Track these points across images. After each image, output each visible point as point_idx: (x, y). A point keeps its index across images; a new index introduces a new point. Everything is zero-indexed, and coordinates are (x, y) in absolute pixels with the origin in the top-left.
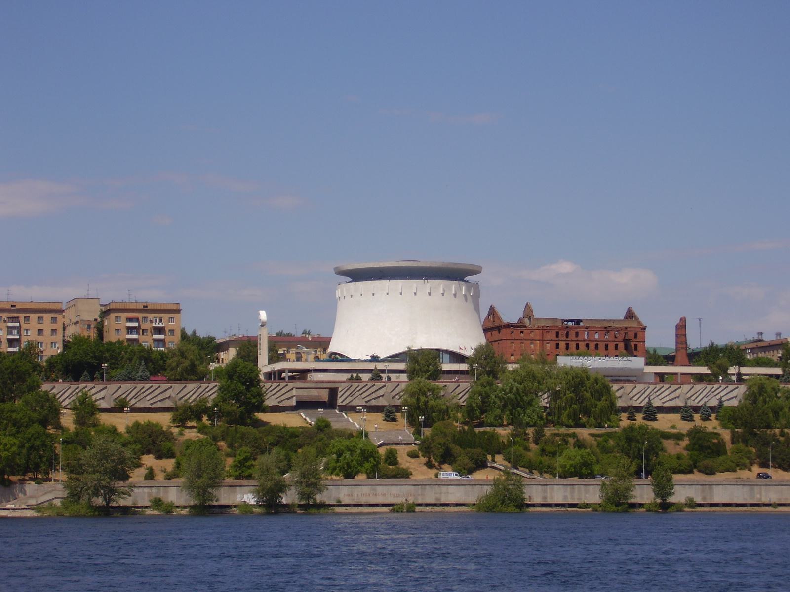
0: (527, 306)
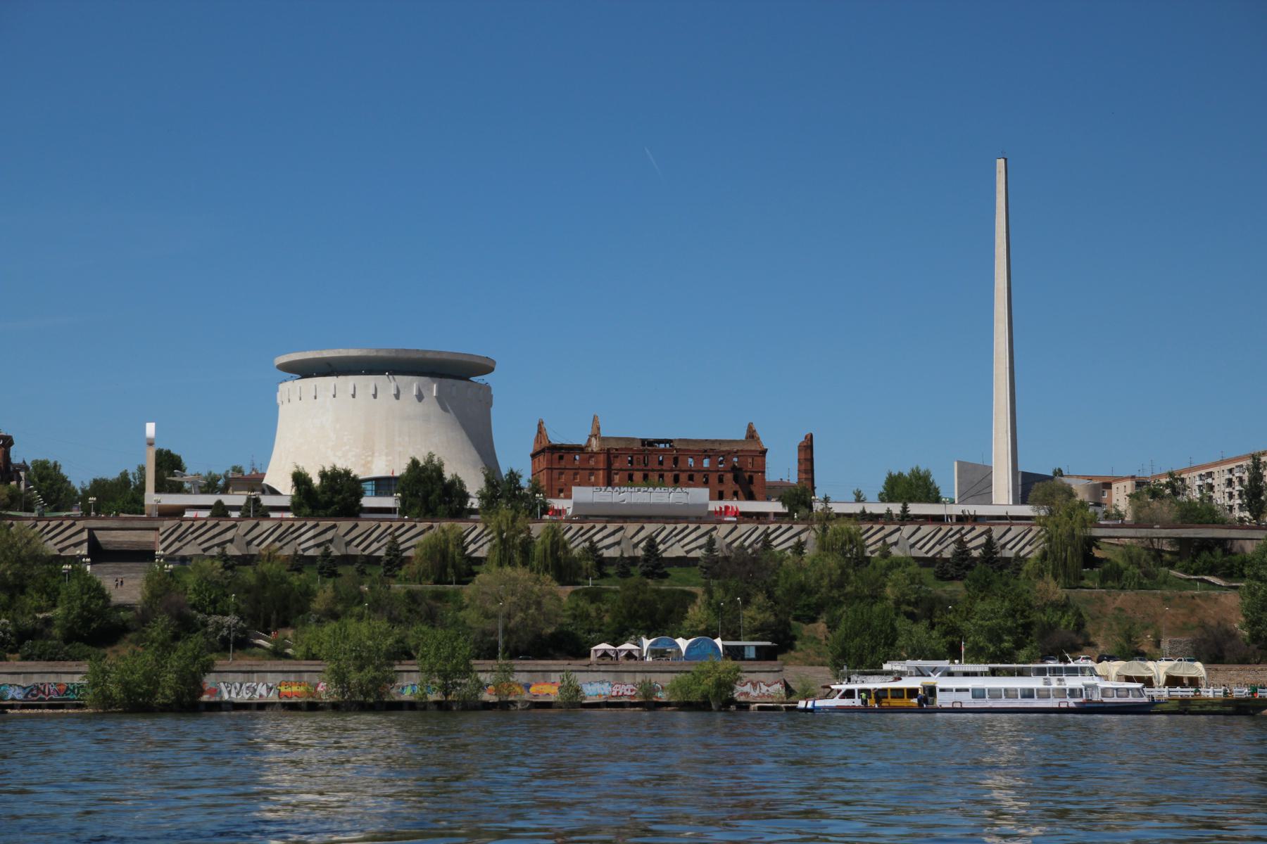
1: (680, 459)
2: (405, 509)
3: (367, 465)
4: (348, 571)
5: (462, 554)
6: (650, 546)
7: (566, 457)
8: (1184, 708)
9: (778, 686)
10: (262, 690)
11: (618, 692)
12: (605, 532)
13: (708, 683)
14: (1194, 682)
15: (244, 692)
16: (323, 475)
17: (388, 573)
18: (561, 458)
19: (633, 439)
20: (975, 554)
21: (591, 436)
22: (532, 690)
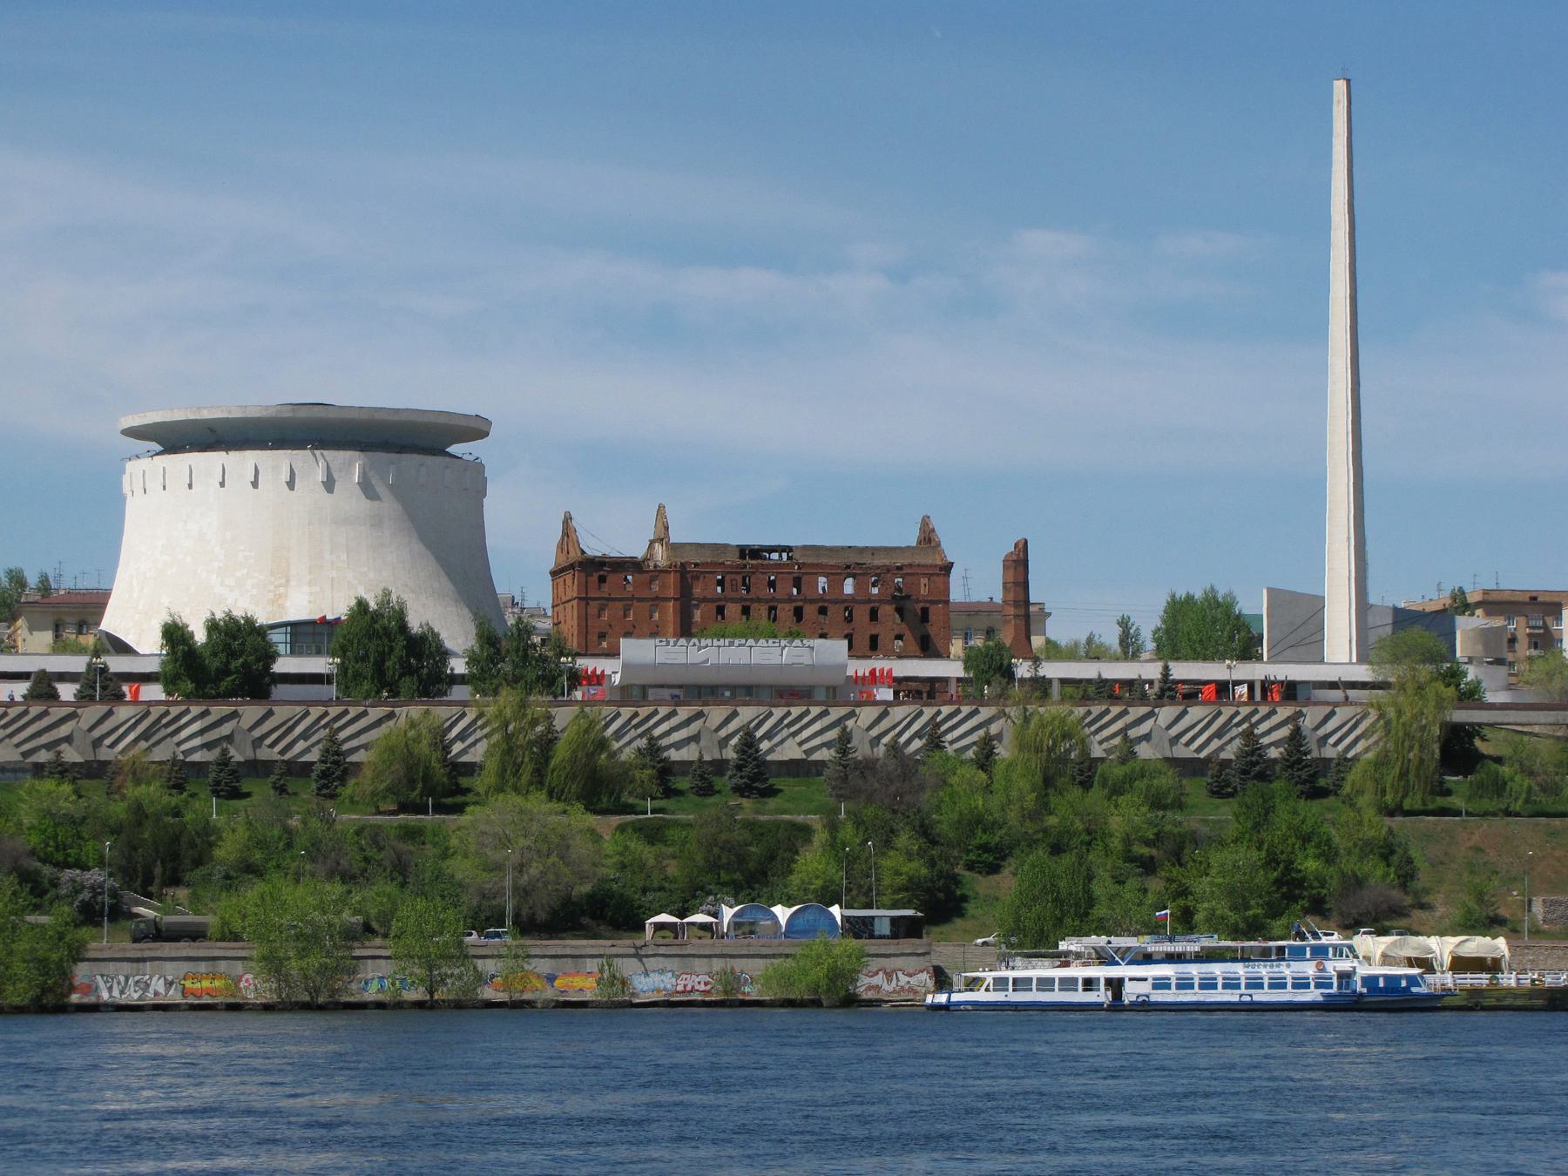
0: (925, 522)
1: (803, 579)
2: (347, 680)
3: (278, 599)
4: (260, 790)
5: (444, 761)
6: (746, 745)
7: (611, 578)
8: (1474, 1002)
9: (924, 976)
10: (158, 985)
11: (685, 986)
12: (674, 721)
13: (818, 973)
14: (1491, 966)
15: (132, 989)
16: (212, 626)
17: (324, 791)
18: (602, 580)
19: (726, 546)
20: (1274, 753)
21: (652, 542)
22: (557, 983)
